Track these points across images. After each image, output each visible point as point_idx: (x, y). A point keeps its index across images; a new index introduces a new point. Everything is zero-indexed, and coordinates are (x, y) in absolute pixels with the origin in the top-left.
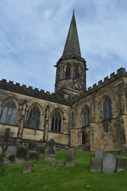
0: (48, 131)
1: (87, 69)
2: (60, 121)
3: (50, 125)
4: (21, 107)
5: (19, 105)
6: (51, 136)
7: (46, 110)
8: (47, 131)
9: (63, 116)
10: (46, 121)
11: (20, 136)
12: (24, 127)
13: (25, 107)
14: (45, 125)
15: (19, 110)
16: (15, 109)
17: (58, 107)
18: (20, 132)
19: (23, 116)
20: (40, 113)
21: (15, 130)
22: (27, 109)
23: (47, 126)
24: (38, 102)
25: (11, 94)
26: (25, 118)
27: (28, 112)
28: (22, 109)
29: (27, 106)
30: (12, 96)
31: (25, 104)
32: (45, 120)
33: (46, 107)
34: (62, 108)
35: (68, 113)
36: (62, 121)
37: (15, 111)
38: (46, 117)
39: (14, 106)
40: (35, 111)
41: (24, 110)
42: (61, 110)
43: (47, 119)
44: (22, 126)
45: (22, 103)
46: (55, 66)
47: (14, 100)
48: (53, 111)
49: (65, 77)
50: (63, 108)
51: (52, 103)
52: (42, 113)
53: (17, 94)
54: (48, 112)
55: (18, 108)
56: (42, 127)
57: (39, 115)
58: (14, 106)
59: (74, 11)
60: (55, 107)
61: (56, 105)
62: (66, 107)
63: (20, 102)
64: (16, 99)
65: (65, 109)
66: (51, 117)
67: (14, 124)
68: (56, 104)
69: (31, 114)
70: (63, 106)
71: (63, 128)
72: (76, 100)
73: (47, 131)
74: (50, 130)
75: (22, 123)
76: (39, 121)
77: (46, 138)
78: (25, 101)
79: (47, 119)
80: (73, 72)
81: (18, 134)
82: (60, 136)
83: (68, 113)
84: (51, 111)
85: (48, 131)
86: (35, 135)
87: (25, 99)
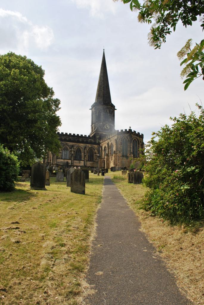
0: (87, 161)
1: (116, 109)
2: (93, 154)
3: (87, 158)
4: (71, 150)
5: (70, 148)
6: (89, 164)
7: (84, 150)
8: (85, 161)
9: (94, 152)
10: (85, 156)
11: (72, 164)
12: (74, 160)
13: (73, 149)
14: (84, 158)
15: (70, 151)
16: (68, 151)
17: (91, 147)
18: (72, 162)
19: (73, 154)
20: (81, 151)
21: (70, 161)
22: (74, 150)
23: (86, 158)
24: (79, 145)
25: (65, 143)
26: (74, 155)
27: (75, 152)
28: (72, 151)
29: (74, 149)
30: (65, 144)
31: (73, 148)
32: (84, 155)
33: (84, 148)
34: (93, 147)
35: (97, 150)
36: (94, 154)
37: (68, 152)
38: (84, 153)
39: (67, 150)
40: (79, 151)
41: (73, 151)
42: (94, 148)
43: (85, 154)
44: (73, 159)
45: (71, 147)
46: (90, 109)
47: (67, 146)
48: (88, 149)
49: (97, 120)
50: (95, 147)
51: (88, 145)
52: (82, 151)
53: (68, 143)
54: (85, 151)
55: (69, 150)
56: (83, 159)
57: (81, 152)
58: (67, 150)
59: (104, 50)
60: (89, 147)
61: (89, 146)
62: (96, 146)
63: (70, 147)
64: (68, 145)
65: (96, 147)
66: (87, 153)
67: (68, 159)
68: (90, 145)
69: (76, 152)
70: (94, 146)
71: (95, 158)
72: (102, 142)
73: (85, 161)
74: (87, 160)
75: (73, 158)
76: (81, 156)
77: (85, 165)
78: (73, 146)
79: (85, 154)
80: (102, 117)
81: (72, 163)
82: (93, 163)
83: (97, 150)
84: (87, 150)
85: (87, 161)
86: (80, 163)
87: (72, 145)
